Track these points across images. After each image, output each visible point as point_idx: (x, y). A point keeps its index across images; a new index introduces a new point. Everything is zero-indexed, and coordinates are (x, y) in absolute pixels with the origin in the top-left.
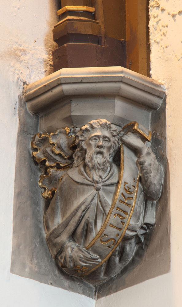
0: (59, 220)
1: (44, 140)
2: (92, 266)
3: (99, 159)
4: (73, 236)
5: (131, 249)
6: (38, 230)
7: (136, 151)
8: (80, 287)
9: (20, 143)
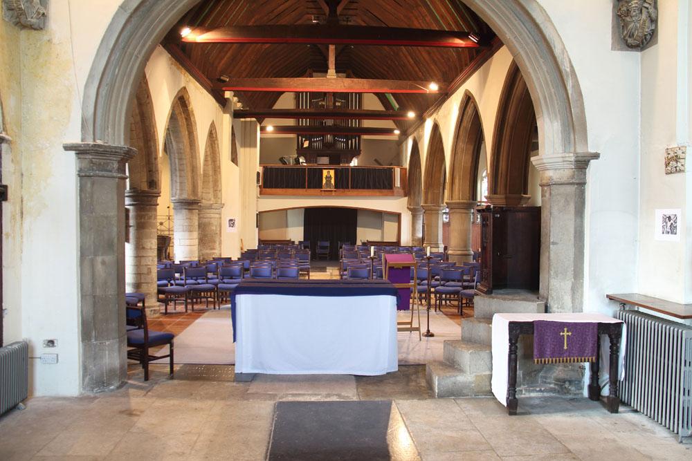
0: (626, 32)
1: (620, 9)
2: (563, 349)
3: (634, 13)
4: (630, 37)
5: (648, 37)
6: (620, 35)
7: (647, 8)
8: (529, 446)
9: (613, 11)
